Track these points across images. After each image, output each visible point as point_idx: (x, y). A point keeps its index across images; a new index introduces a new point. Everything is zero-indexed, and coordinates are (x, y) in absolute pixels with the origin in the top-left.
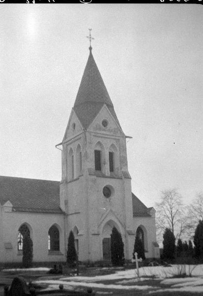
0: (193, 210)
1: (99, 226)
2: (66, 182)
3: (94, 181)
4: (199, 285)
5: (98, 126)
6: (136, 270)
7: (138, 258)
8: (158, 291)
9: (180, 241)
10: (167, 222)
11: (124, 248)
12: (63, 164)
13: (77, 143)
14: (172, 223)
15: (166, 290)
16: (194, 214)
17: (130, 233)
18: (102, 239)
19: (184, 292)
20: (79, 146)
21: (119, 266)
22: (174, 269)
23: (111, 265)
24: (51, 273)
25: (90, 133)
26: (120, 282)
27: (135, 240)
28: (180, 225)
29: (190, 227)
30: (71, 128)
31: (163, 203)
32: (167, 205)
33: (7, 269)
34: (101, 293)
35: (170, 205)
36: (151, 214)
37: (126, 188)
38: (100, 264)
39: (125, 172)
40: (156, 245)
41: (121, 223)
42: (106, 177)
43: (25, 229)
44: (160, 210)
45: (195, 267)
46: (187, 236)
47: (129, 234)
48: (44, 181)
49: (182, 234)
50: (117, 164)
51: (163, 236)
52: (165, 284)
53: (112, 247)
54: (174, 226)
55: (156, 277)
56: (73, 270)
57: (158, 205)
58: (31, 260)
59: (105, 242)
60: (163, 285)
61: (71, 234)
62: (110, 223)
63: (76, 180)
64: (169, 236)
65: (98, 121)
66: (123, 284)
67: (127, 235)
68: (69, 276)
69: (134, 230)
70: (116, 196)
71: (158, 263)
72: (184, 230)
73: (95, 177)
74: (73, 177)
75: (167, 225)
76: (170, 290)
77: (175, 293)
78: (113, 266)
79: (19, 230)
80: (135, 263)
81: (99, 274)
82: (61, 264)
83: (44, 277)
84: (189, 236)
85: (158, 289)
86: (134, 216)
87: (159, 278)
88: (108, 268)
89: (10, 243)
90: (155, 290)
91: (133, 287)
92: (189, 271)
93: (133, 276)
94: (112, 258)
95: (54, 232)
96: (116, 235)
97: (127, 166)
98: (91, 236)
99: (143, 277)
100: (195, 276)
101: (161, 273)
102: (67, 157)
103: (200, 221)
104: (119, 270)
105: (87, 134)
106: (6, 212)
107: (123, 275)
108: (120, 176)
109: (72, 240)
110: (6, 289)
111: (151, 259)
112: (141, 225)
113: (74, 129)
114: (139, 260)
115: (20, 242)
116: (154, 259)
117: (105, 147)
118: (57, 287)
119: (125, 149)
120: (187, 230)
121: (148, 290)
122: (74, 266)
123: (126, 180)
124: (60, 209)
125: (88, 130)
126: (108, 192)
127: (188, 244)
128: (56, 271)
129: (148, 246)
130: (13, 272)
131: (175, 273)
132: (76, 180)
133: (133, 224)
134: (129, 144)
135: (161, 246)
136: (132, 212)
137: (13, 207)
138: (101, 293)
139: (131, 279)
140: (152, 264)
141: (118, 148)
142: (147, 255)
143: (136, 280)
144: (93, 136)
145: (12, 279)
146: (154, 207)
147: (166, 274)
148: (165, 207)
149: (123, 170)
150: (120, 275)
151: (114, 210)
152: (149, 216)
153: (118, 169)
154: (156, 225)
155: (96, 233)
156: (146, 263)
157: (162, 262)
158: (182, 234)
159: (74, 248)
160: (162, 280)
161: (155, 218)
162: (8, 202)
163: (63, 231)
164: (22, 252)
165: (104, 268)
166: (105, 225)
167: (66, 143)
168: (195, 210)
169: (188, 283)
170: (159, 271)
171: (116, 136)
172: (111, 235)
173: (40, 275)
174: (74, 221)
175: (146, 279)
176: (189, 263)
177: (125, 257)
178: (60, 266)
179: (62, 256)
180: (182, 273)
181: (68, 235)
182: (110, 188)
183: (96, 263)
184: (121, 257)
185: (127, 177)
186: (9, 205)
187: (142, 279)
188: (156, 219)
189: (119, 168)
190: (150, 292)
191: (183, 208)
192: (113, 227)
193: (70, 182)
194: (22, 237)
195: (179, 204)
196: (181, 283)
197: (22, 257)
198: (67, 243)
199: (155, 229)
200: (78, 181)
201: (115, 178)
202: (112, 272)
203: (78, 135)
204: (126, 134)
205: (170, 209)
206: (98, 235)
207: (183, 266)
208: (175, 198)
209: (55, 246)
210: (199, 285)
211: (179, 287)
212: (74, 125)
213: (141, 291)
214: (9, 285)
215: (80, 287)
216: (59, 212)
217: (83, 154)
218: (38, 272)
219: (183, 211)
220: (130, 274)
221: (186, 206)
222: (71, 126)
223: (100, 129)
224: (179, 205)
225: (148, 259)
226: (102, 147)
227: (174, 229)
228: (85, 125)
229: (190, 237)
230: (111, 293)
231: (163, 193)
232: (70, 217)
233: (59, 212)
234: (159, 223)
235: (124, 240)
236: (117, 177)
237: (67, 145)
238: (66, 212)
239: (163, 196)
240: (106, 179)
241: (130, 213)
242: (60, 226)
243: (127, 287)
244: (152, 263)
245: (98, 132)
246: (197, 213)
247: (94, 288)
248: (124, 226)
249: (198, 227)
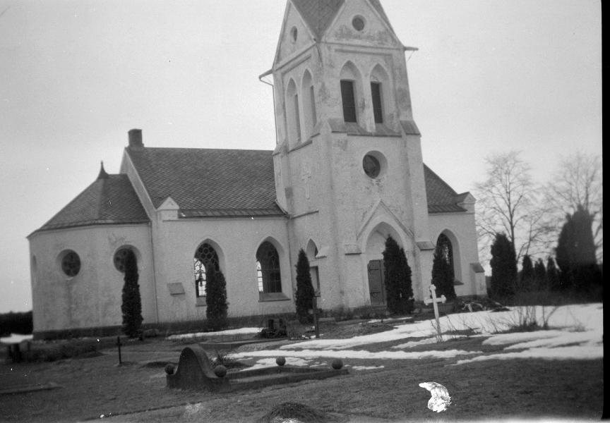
0: (554, 195)
1: (359, 235)
2: (285, 150)
3: (344, 145)
4: (563, 346)
5: (344, 29)
6: (434, 321)
7: (438, 296)
8: (475, 359)
9: (527, 260)
10: (500, 222)
11: (413, 278)
12: (277, 113)
13: (303, 68)
14: (511, 223)
15: (492, 356)
16: (558, 202)
17: (423, 248)
18: (366, 263)
19: (531, 358)
20: (307, 74)
21: (403, 314)
22: (514, 315)
23: (387, 313)
24: (263, 336)
25: (329, 45)
26: (401, 346)
27: (434, 261)
28: (527, 226)
29: (548, 229)
30: (289, 37)
31: (491, 184)
32: (499, 185)
33: (176, 334)
34: (361, 368)
35: (506, 187)
36: (465, 207)
37: (411, 156)
38: (364, 314)
39: (406, 122)
40: (478, 269)
41: (405, 230)
42: (370, 135)
43: (207, 253)
44: (485, 196)
45: (554, 310)
46: (542, 248)
47: (422, 250)
48: (241, 153)
49: (532, 244)
50: (389, 106)
51: (490, 250)
52: (493, 344)
53: (387, 277)
54: (515, 229)
55: (475, 331)
56: (308, 329)
57: (480, 187)
58: (225, 313)
59: (372, 267)
60: (489, 346)
61: (303, 257)
62: (380, 229)
63: (309, 143)
64: (503, 249)
65: (343, 19)
66: (407, 350)
67: (418, 250)
68: (300, 339)
69: (432, 241)
70: (390, 171)
71: (481, 305)
72: (536, 236)
73: (343, 136)
74: (299, 140)
75: (500, 228)
76: (502, 356)
77: (509, 361)
78: (391, 316)
79: (196, 256)
80: (431, 305)
81: (360, 333)
82: (283, 318)
83: (250, 345)
84: (547, 247)
85: (477, 355)
86: (429, 212)
87: (480, 333)
88: (380, 321)
89: (179, 284)
90: (470, 357)
91: (426, 354)
92: (543, 317)
93: (428, 333)
94: (388, 299)
95: (268, 254)
96: (394, 254)
97: (411, 110)
98: (343, 257)
99: (448, 333)
100: (554, 328)
101: (484, 322)
102: (284, 99)
103: (568, 216)
104: (401, 322)
105: (324, 49)
106: (164, 221)
107: (409, 333)
108: (397, 131)
109: (303, 268)
110: (170, 372)
111: (469, 297)
112: (446, 230)
113: (295, 39)
114: (439, 300)
115: (201, 279)
116: (475, 297)
117: (361, 72)
118: (272, 363)
119: (404, 76)
120: (544, 237)
121: (458, 357)
122: (310, 321)
123: (411, 139)
124: (278, 207)
125: (323, 40)
126: (373, 165)
127: (546, 264)
128: (275, 330)
129: (463, 271)
130: (189, 339)
131: (512, 322)
132: (309, 143)
133: (428, 229)
134: (411, 60)
135: (488, 271)
136: (425, 205)
137: (181, 211)
138: (361, 368)
139: (425, 338)
140: (470, 309)
141: (389, 74)
142: (460, 291)
143: (434, 340)
144: (336, 50)
145: (180, 353)
146: (472, 193)
147: (494, 324)
148: (494, 190)
149: (402, 118)
150: (402, 333)
151: (388, 203)
152: (462, 210)
153: (392, 116)
154: (478, 228)
155: (354, 252)
156: (456, 305)
157: (490, 302)
158: (532, 244)
159: (309, 282)
160: (487, 338)
161: (473, 213)
162: (169, 199)
163: (286, 251)
164: (204, 300)
165: (373, 321)
166: (370, 238)
167: (281, 68)
168: (559, 193)
169: (538, 342)
170: (481, 321)
171: (382, 48)
172: (384, 253)
173: (243, 342)
174: (306, 229)
175: (454, 337)
176: (545, 303)
177: (415, 297)
178: (281, 321)
179: (286, 303)
180: (528, 321)
181: (296, 261)
182: (375, 156)
183: (357, 311)
184: (405, 298)
185: (411, 131)
186: (170, 207)
187: (446, 338)
188: (476, 215)
189: (395, 114)
190: (460, 362)
191: (534, 191)
192: (387, 237)
193: (293, 150)
194: (203, 268)
195: (525, 183)
196: (530, 340)
197: (205, 309)
198: (295, 275)
199: (474, 237)
200: (309, 148)
201: (385, 136)
202: (388, 327)
203: (304, 52)
204: (406, 44)
205: (504, 196)
206: (359, 254)
207: (531, 308)
208: (515, 171)
209: (273, 283)
210: (563, 346)
211: (520, 350)
212: (295, 32)
213: (442, 359)
214: (175, 364)
215: (320, 359)
216: (275, 211)
217: (316, 91)
218: (239, 336)
219: (532, 197)
220: (423, 328)
221: (539, 186)
222: (289, 33)
223: (349, 35)
224: (524, 185)
225: (461, 298)
226: (356, 72)
227: (516, 235)
228: (318, 32)
229: (548, 250)
230: (382, 367)
231: (489, 161)
232: (299, 222)
233: (275, 211)
234: (483, 224)
235: (410, 263)
236: (391, 134)
237: (283, 74)
238: (290, 213)
239: (491, 167)
240: (440, 326)
241: (421, 206)
242: (280, 243)
243: (415, 355)
244: (469, 306)
245: (344, 41)
246: (562, 200)
247: (348, 360)
248: (411, 234)
249: (565, 228)
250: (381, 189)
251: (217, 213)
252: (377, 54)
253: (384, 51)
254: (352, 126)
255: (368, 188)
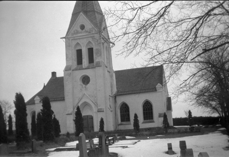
126: (86, 80)
155: (70, 113)
245: (75, 36)
250: (86, 89)
251: (144, 91)
252: (88, 37)
253: (91, 36)
254: (80, 66)
255: (81, 89)
